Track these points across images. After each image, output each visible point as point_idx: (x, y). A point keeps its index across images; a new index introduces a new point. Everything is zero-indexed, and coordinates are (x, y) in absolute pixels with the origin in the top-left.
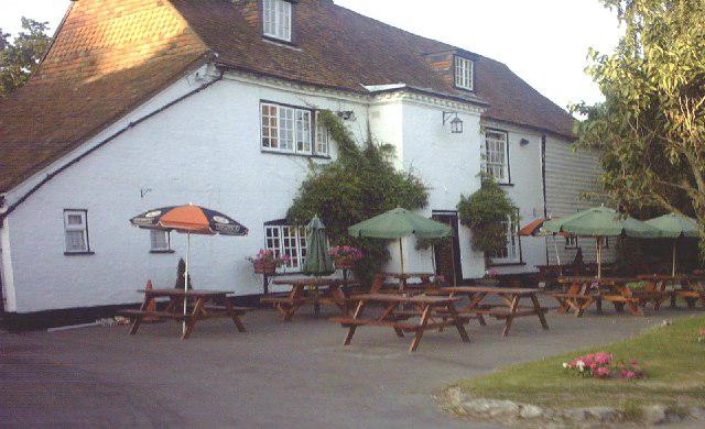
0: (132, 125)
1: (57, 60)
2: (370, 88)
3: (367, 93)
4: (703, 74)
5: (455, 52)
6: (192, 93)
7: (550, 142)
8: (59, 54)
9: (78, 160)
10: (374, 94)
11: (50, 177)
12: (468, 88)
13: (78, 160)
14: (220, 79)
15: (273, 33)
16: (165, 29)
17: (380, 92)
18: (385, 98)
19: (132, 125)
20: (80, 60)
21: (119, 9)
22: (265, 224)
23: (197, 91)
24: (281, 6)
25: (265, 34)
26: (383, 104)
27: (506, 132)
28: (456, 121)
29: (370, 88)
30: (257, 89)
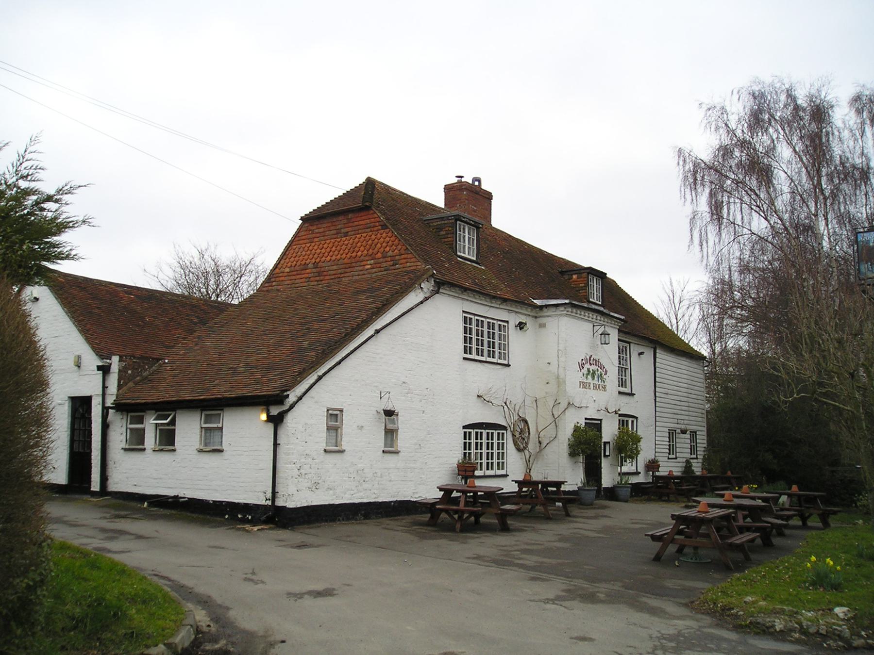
0: (378, 332)
1: (287, 270)
2: (538, 302)
3: (535, 306)
4: (873, 226)
5: (588, 271)
6: (418, 305)
7: (660, 354)
8: (289, 265)
9: (339, 363)
10: (541, 307)
11: (320, 378)
12: (598, 302)
13: (339, 363)
14: (437, 292)
15: (464, 253)
16: (388, 248)
17: (547, 306)
18: (550, 312)
19: (378, 332)
20: (308, 271)
21: (346, 230)
22: (464, 427)
23: (422, 302)
24: (469, 229)
25: (458, 253)
26: (548, 316)
27: (629, 343)
28: (604, 334)
29: (538, 302)
30: (460, 302)
